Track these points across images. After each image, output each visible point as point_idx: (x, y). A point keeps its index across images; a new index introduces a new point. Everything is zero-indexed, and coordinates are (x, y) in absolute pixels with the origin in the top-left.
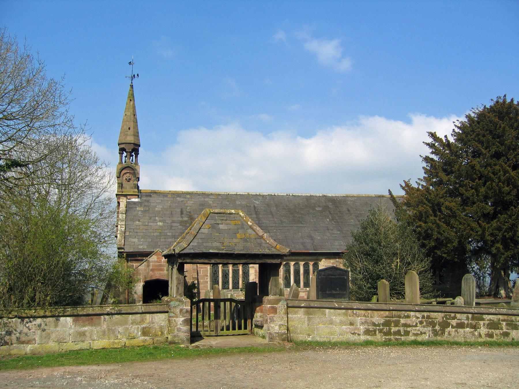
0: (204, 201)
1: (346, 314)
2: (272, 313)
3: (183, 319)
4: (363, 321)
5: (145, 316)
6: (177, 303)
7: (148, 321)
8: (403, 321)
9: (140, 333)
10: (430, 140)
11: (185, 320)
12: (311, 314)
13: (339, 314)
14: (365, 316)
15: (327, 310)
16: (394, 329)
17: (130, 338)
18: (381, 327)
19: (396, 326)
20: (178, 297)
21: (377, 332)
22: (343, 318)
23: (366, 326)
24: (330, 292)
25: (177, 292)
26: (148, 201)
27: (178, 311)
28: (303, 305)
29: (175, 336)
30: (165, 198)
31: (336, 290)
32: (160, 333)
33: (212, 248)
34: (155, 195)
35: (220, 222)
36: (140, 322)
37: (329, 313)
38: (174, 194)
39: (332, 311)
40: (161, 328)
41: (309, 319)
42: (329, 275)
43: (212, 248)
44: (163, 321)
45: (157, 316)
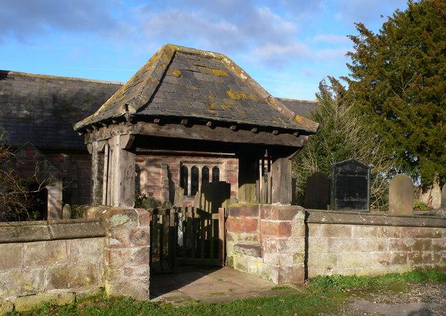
0: (82, 90)
1: (374, 233)
2: (284, 234)
3: (137, 249)
4: (393, 242)
5: (57, 246)
6: (125, 218)
7: (62, 256)
8: (434, 242)
9: (46, 282)
10: (357, 34)
11: (139, 252)
12: (334, 235)
13: (367, 234)
14: (395, 235)
15: (353, 227)
16: (425, 253)
17: (26, 293)
18: (412, 251)
19: (427, 249)
20: (125, 206)
21: (408, 258)
22: (369, 239)
23: (396, 251)
24: (348, 200)
25: (123, 195)
26: (10, 85)
27: (125, 235)
28: (323, 220)
29: (120, 286)
30: (32, 83)
31: (355, 197)
32: (88, 279)
33: (196, 111)
34: (18, 78)
35: (194, 68)
36: (46, 259)
37: (356, 231)
38: (43, 79)
39: (359, 227)
40: (91, 268)
41: (330, 242)
42: (347, 172)
43: (196, 111)
44: (94, 254)
45: (83, 245)
